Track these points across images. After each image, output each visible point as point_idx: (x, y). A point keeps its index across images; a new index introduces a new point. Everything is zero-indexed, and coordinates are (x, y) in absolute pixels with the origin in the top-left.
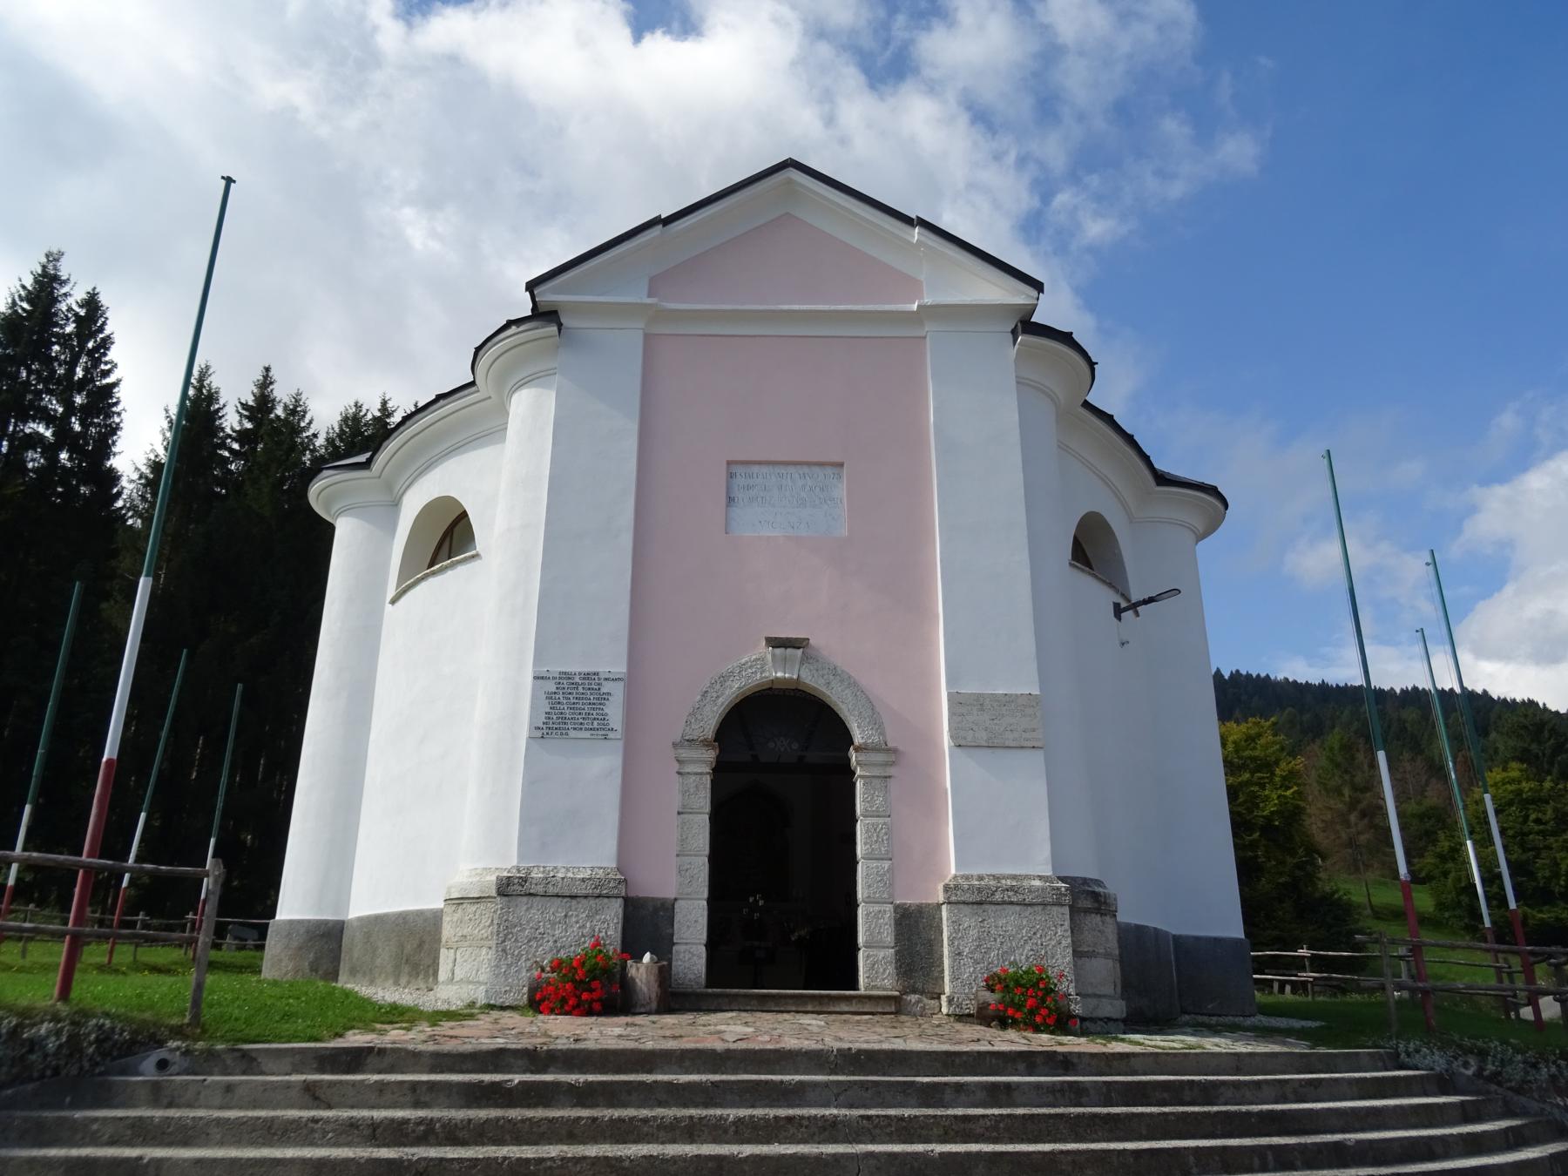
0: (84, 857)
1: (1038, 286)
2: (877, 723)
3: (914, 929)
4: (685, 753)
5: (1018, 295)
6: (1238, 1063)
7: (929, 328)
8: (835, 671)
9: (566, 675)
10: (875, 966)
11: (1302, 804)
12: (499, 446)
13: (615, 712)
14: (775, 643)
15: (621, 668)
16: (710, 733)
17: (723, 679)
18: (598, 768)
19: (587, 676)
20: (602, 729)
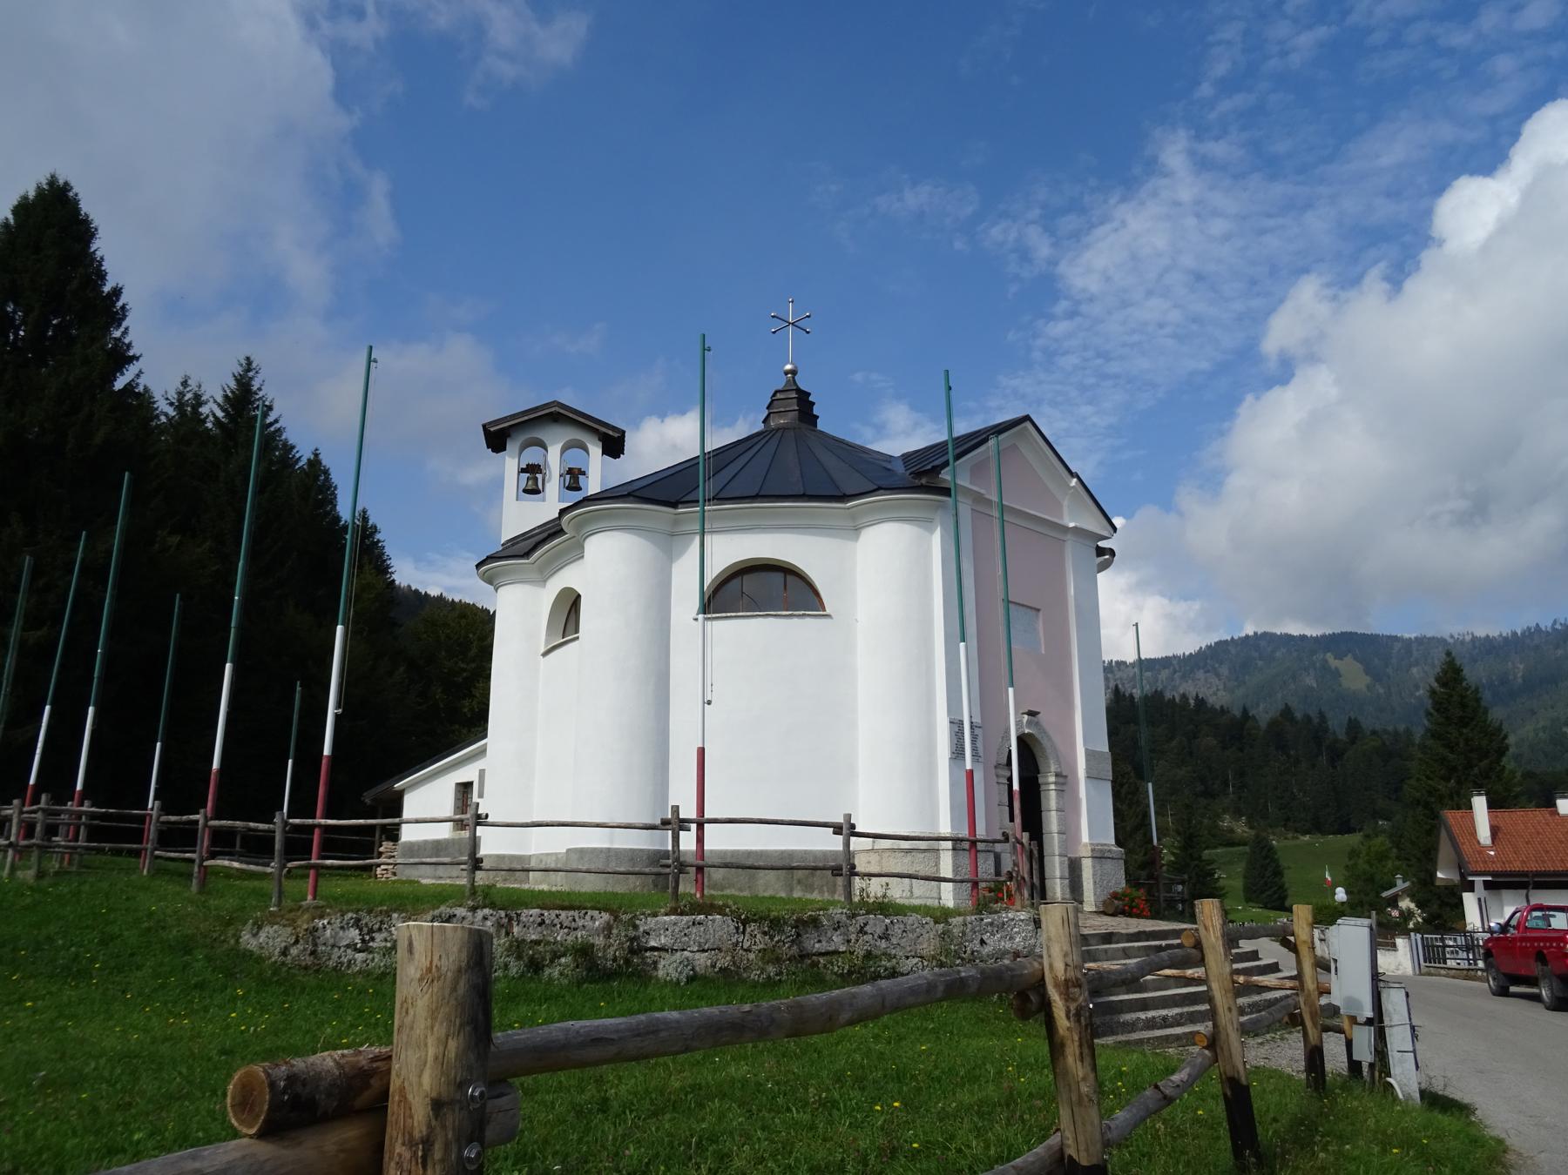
2: (1058, 762)
3: (1074, 867)
7: (1069, 536)
11: (1084, 819)
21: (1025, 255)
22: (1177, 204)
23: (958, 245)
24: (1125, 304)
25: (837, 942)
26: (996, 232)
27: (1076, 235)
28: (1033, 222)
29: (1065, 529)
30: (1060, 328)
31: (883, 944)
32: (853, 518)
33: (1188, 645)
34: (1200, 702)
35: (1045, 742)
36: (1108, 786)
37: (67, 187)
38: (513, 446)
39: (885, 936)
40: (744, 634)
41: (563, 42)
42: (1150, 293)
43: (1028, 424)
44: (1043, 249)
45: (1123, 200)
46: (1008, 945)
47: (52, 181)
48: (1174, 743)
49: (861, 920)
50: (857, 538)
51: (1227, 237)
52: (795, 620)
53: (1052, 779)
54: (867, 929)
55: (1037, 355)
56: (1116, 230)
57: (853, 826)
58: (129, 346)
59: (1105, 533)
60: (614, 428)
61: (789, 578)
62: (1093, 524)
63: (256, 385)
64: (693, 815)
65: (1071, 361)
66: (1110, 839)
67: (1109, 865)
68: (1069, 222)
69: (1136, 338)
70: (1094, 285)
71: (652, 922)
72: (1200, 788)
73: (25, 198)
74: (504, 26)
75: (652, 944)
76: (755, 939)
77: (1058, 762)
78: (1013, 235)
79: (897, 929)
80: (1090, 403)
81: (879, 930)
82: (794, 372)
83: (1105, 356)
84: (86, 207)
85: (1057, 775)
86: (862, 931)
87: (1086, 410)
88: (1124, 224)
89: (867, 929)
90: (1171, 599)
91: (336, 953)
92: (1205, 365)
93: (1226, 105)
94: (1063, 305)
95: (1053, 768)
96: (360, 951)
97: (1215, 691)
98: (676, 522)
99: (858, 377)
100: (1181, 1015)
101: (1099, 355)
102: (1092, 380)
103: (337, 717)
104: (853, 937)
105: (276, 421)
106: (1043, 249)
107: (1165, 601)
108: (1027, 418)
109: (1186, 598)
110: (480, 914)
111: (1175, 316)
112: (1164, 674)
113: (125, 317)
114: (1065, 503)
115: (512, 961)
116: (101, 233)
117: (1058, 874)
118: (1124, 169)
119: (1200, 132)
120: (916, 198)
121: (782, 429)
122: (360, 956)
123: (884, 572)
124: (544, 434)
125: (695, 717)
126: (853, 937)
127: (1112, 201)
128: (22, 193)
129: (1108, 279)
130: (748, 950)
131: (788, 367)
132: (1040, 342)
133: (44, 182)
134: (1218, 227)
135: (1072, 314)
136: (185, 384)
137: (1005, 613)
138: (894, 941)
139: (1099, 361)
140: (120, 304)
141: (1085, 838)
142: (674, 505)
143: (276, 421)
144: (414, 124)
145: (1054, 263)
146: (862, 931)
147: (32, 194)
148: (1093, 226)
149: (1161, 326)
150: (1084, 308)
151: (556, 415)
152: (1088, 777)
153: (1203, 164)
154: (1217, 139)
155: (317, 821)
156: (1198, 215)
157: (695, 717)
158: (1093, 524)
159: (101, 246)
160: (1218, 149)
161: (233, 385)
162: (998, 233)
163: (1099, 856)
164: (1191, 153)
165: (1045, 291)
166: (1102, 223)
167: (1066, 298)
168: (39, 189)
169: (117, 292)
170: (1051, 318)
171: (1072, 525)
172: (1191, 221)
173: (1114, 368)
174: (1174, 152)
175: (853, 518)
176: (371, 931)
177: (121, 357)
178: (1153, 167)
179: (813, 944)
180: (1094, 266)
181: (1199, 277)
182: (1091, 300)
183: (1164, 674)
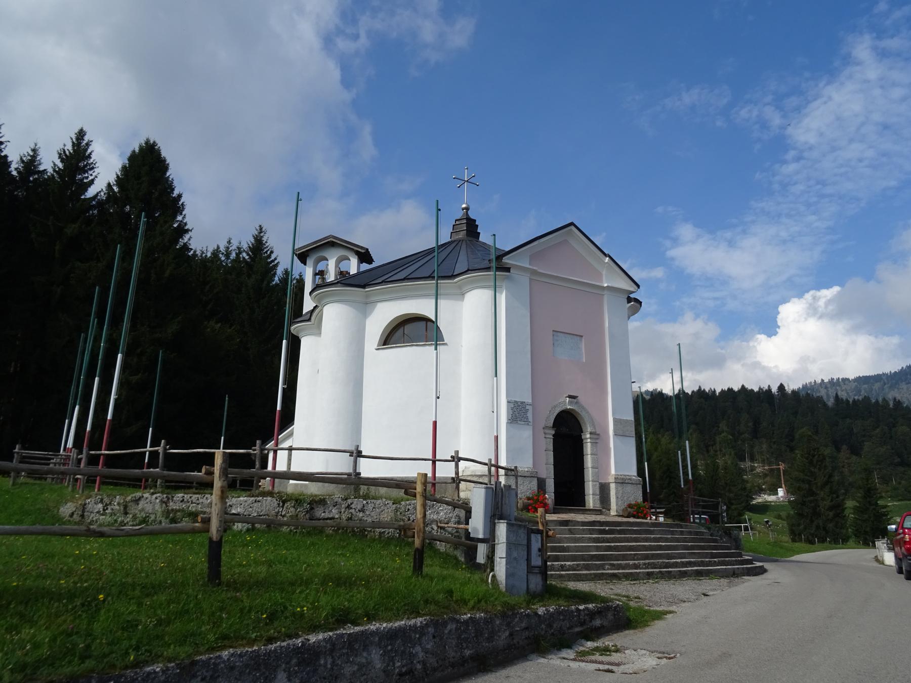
0: (100, 467)
1: (638, 286)
2: (593, 425)
3: (604, 490)
4: (547, 431)
5: (632, 288)
6: (578, 578)
7: (605, 292)
8: (583, 407)
9: (516, 402)
10: (591, 501)
11: (613, 461)
12: (460, 302)
13: (530, 415)
14: (570, 397)
15: (530, 401)
16: (551, 425)
17: (555, 407)
18: (526, 434)
19: (522, 403)
20: (527, 421)
21: (764, 125)
22: (867, 81)
23: (719, 123)
24: (834, 149)
25: (334, 512)
26: (744, 113)
27: (798, 109)
28: (768, 104)
29: (603, 288)
30: (792, 168)
31: (361, 514)
32: (460, 288)
33: (892, 366)
34: (898, 403)
35: (583, 414)
36: (634, 439)
37: (154, 144)
38: (310, 261)
39: (362, 510)
40: (412, 356)
41: (461, 34)
42: (851, 141)
43: (573, 228)
44: (776, 120)
45: (829, 83)
46: (435, 517)
47: (147, 142)
48: (878, 430)
49: (349, 501)
50: (463, 300)
51: (904, 99)
52: (428, 347)
53: (588, 436)
54: (353, 506)
55: (776, 187)
56: (825, 103)
57: (360, 452)
58: (186, 224)
59: (632, 289)
60: (362, 248)
61: (429, 323)
62: (624, 284)
63: (264, 239)
64: (486, 468)
65: (801, 187)
66: (633, 471)
67: (629, 488)
68: (793, 101)
69: (843, 170)
70: (812, 139)
71: (234, 500)
72: (897, 460)
73: (134, 151)
74: (428, 31)
75: (233, 512)
76: (289, 510)
77: (593, 425)
78: (755, 113)
79: (370, 506)
80: (814, 214)
81: (359, 507)
82: (467, 209)
83: (823, 183)
84: (164, 154)
85: (591, 433)
86: (349, 507)
87: (812, 218)
88: (830, 98)
89: (353, 506)
90: (876, 337)
91: (92, 515)
92: (893, 183)
93: (898, 14)
94: (792, 154)
95: (589, 430)
96: (103, 515)
97: (876, 394)
98: (367, 297)
99: (660, 209)
100: (578, 565)
101: (818, 183)
102: (815, 199)
103: (116, 400)
104: (343, 510)
105: (275, 259)
106: (776, 120)
107: (872, 338)
108: (572, 224)
109: (890, 334)
110: (155, 496)
111: (870, 153)
112: (877, 386)
113: (183, 209)
114: (604, 273)
115: (163, 520)
116: (171, 167)
117: (591, 492)
118: (828, 62)
119: (880, 33)
120: (689, 98)
121: (459, 241)
122: (102, 517)
123: (472, 314)
124: (326, 253)
125: (399, 402)
126: (343, 510)
127: (821, 85)
128: (132, 149)
129: (821, 135)
130: (283, 516)
131: (464, 206)
132: (777, 178)
133: (143, 142)
134: (897, 93)
135: (798, 159)
136: (229, 242)
137: (550, 337)
138: (367, 513)
139: (819, 187)
140: (180, 203)
141: (613, 472)
142: (364, 287)
143: (275, 259)
144: (387, 91)
145: (783, 128)
146: (349, 507)
147: (137, 150)
148: (808, 102)
149: (860, 160)
150: (806, 154)
151: (331, 243)
152: (616, 435)
153: (882, 54)
154: (892, 37)
155: (103, 452)
156: (882, 87)
157: (399, 402)
158: (624, 284)
159: (172, 173)
160: (893, 43)
161: (253, 240)
162: (744, 113)
163: (622, 482)
164: (875, 49)
165: (779, 146)
166: (815, 99)
167: (794, 149)
168: (141, 148)
169: (180, 196)
170: (785, 162)
171: (606, 285)
172: (877, 92)
173: (829, 190)
174: (862, 49)
175: (460, 288)
176: (107, 505)
177: (182, 230)
178: (848, 60)
179: (320, 513)
180: (811, 127)
181: (886, 127)
182: (811, 148)
183: (877, 386)
